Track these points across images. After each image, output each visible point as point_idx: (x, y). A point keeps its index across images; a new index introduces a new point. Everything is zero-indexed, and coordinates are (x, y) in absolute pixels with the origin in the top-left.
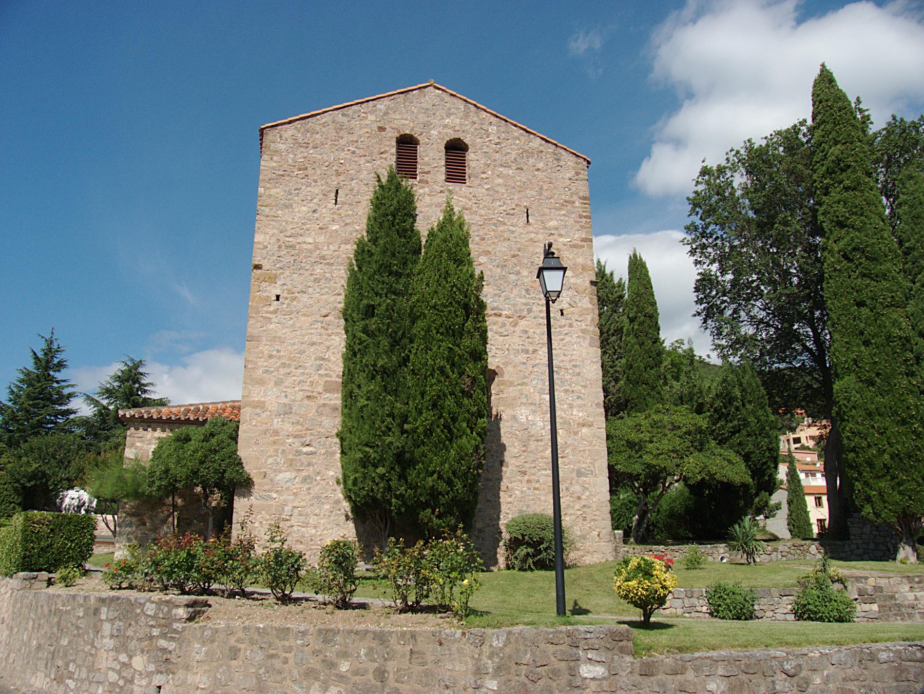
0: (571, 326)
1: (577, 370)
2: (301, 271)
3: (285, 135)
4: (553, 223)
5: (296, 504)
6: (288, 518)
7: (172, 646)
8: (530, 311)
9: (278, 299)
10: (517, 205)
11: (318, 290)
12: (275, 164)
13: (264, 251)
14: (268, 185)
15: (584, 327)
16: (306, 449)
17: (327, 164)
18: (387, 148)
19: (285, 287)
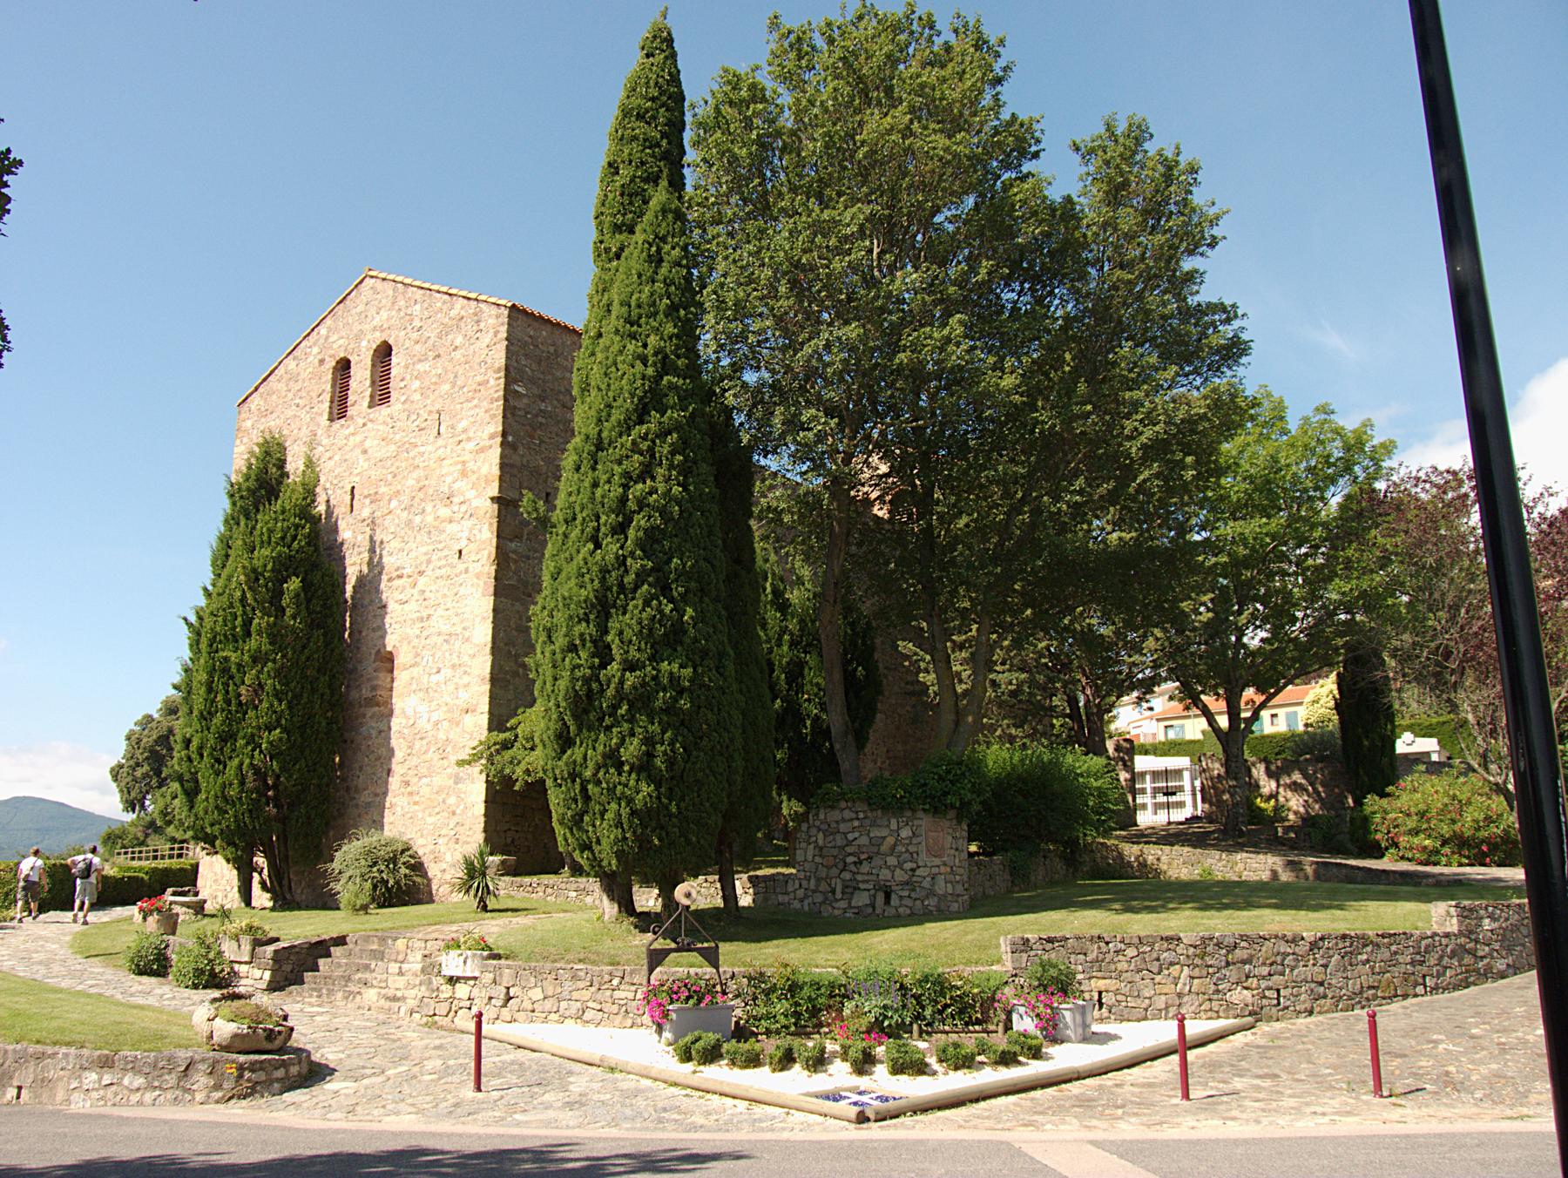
0: (467, 571)
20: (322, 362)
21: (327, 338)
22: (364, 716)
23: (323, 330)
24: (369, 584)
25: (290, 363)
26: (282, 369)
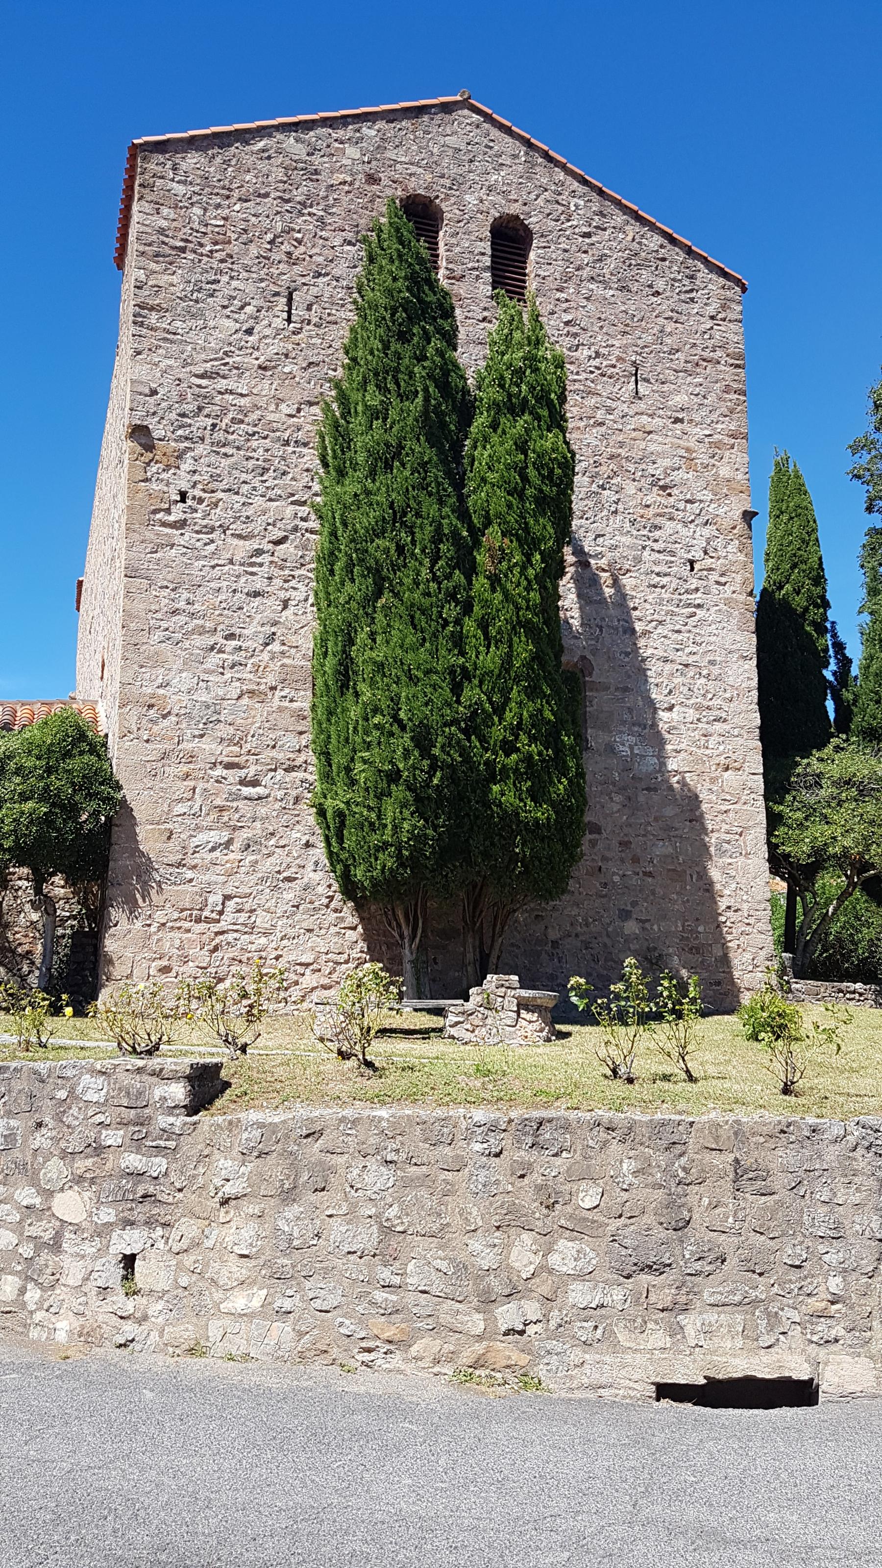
2: (228, 450)
3: (184, 166)
4: (680, 399)
5: (228, 892)
6: (214, 916)
7: (159, 1164)
8: (638, 560)
9: (183, 500)
10: (619, 359)
11: (262, 490)
12: (164, 224)
13: (151, 400)
14: (153, 266)
15: (728, 594)
16: (247, 791)
17: (269, 237)
19: (196, 477)
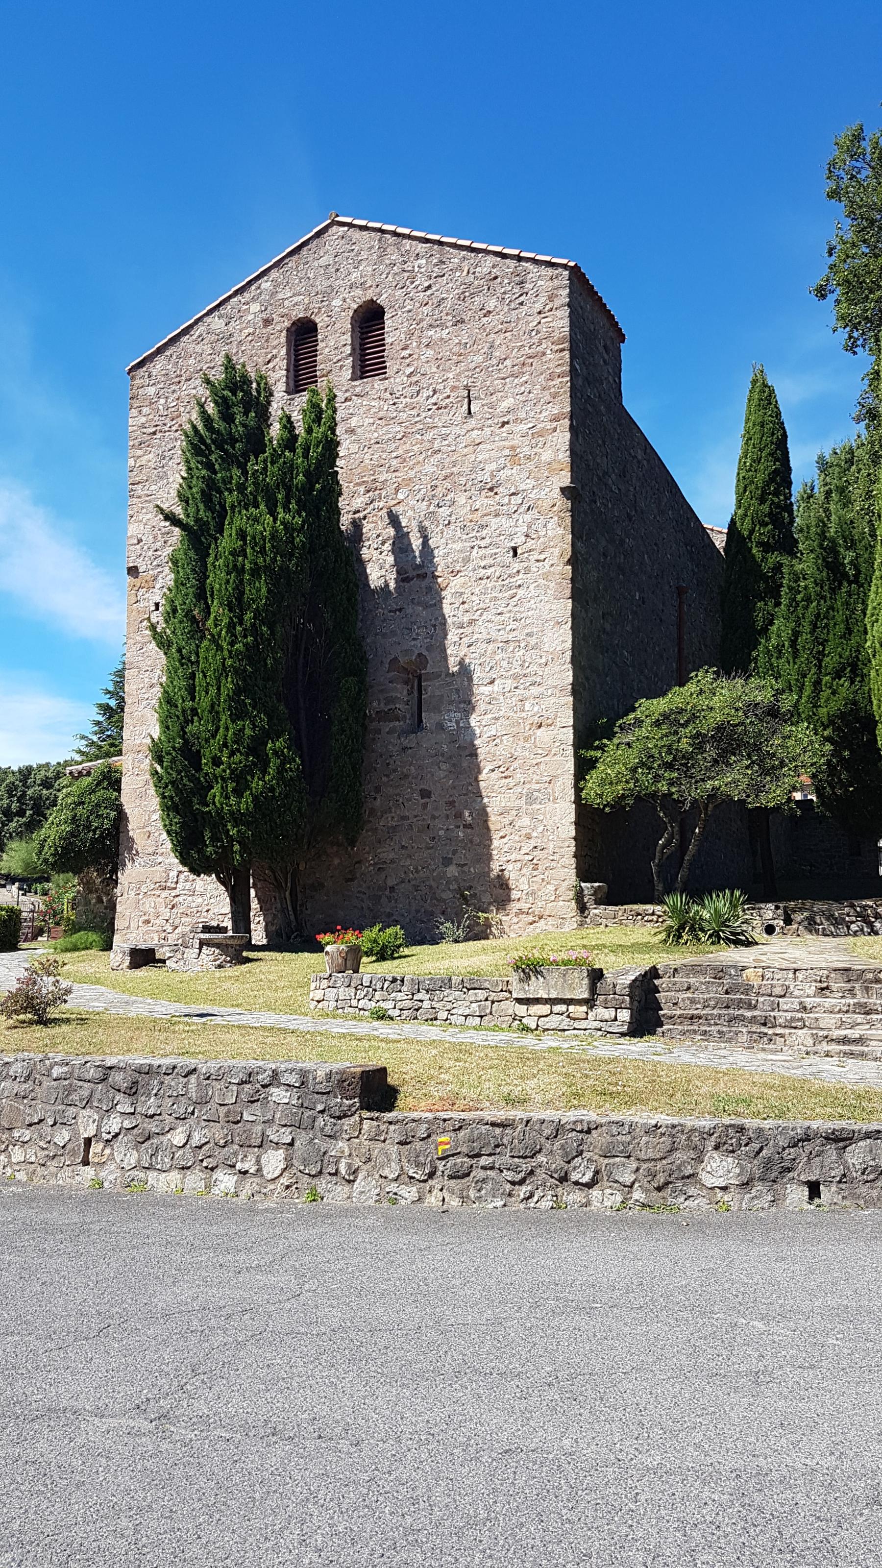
0: (527, 570)
1: (533, 641)
6: (173, 885)
13: (138, 547)
18: (275, 352)
20: (267, 322)
21: (273, 294)
22: (379, 731)
23: (266, 284)
24: (417, 573)
25: (216, 323)
26: (200, 329)
